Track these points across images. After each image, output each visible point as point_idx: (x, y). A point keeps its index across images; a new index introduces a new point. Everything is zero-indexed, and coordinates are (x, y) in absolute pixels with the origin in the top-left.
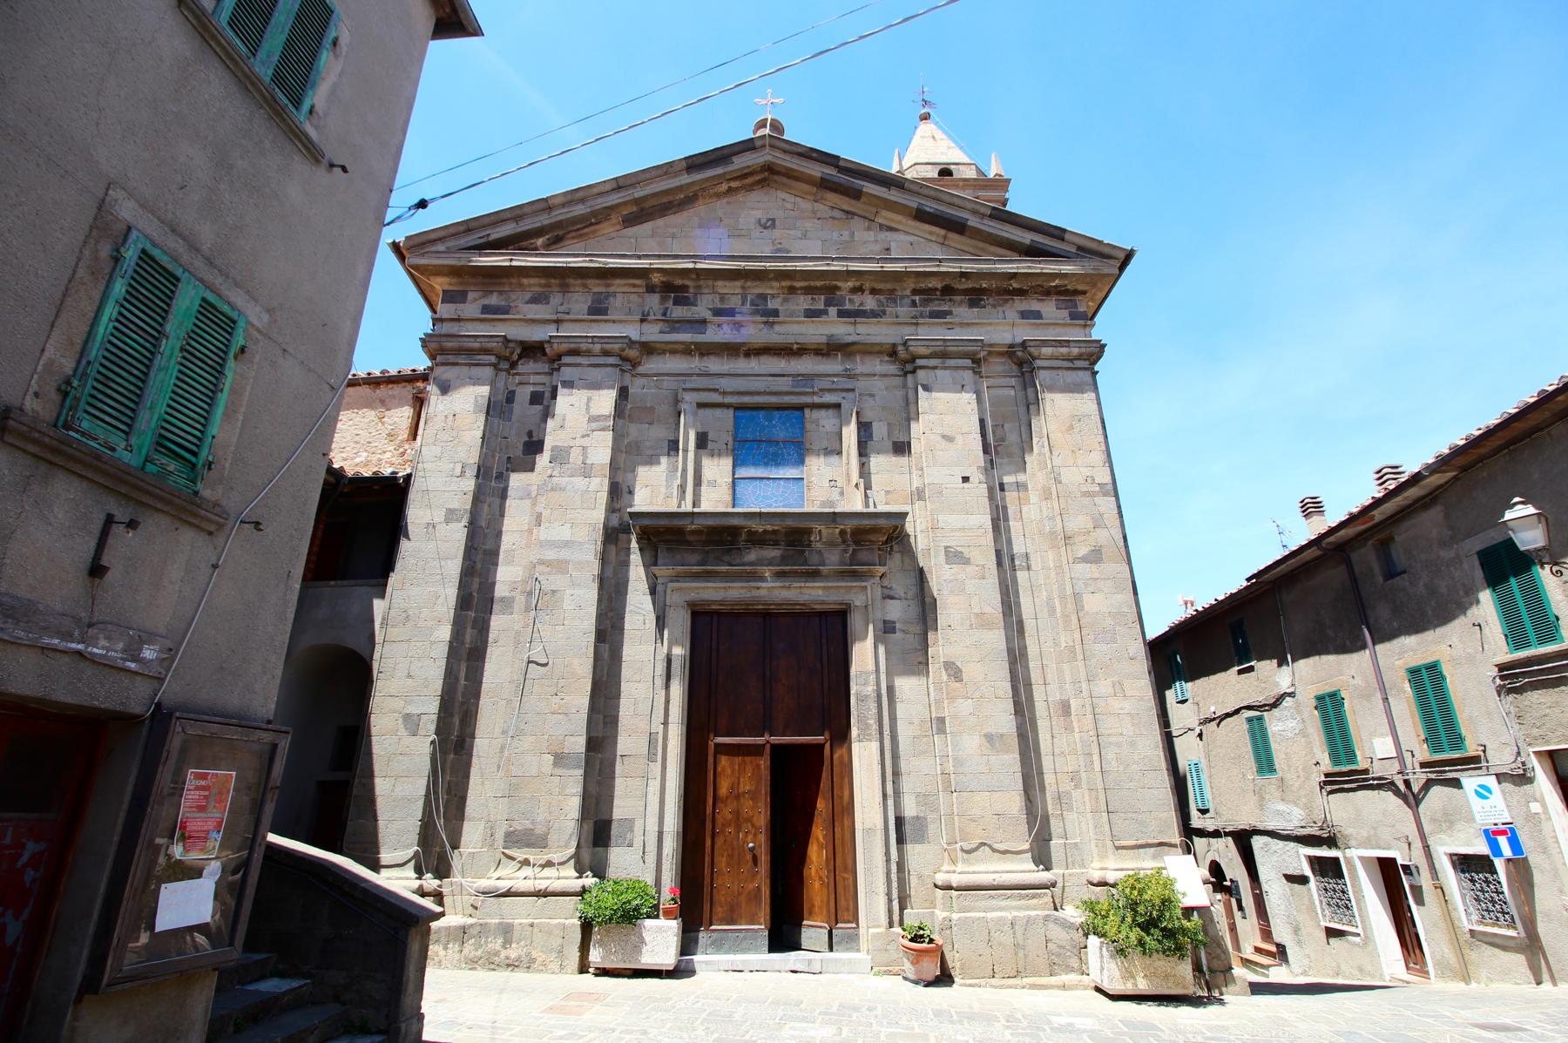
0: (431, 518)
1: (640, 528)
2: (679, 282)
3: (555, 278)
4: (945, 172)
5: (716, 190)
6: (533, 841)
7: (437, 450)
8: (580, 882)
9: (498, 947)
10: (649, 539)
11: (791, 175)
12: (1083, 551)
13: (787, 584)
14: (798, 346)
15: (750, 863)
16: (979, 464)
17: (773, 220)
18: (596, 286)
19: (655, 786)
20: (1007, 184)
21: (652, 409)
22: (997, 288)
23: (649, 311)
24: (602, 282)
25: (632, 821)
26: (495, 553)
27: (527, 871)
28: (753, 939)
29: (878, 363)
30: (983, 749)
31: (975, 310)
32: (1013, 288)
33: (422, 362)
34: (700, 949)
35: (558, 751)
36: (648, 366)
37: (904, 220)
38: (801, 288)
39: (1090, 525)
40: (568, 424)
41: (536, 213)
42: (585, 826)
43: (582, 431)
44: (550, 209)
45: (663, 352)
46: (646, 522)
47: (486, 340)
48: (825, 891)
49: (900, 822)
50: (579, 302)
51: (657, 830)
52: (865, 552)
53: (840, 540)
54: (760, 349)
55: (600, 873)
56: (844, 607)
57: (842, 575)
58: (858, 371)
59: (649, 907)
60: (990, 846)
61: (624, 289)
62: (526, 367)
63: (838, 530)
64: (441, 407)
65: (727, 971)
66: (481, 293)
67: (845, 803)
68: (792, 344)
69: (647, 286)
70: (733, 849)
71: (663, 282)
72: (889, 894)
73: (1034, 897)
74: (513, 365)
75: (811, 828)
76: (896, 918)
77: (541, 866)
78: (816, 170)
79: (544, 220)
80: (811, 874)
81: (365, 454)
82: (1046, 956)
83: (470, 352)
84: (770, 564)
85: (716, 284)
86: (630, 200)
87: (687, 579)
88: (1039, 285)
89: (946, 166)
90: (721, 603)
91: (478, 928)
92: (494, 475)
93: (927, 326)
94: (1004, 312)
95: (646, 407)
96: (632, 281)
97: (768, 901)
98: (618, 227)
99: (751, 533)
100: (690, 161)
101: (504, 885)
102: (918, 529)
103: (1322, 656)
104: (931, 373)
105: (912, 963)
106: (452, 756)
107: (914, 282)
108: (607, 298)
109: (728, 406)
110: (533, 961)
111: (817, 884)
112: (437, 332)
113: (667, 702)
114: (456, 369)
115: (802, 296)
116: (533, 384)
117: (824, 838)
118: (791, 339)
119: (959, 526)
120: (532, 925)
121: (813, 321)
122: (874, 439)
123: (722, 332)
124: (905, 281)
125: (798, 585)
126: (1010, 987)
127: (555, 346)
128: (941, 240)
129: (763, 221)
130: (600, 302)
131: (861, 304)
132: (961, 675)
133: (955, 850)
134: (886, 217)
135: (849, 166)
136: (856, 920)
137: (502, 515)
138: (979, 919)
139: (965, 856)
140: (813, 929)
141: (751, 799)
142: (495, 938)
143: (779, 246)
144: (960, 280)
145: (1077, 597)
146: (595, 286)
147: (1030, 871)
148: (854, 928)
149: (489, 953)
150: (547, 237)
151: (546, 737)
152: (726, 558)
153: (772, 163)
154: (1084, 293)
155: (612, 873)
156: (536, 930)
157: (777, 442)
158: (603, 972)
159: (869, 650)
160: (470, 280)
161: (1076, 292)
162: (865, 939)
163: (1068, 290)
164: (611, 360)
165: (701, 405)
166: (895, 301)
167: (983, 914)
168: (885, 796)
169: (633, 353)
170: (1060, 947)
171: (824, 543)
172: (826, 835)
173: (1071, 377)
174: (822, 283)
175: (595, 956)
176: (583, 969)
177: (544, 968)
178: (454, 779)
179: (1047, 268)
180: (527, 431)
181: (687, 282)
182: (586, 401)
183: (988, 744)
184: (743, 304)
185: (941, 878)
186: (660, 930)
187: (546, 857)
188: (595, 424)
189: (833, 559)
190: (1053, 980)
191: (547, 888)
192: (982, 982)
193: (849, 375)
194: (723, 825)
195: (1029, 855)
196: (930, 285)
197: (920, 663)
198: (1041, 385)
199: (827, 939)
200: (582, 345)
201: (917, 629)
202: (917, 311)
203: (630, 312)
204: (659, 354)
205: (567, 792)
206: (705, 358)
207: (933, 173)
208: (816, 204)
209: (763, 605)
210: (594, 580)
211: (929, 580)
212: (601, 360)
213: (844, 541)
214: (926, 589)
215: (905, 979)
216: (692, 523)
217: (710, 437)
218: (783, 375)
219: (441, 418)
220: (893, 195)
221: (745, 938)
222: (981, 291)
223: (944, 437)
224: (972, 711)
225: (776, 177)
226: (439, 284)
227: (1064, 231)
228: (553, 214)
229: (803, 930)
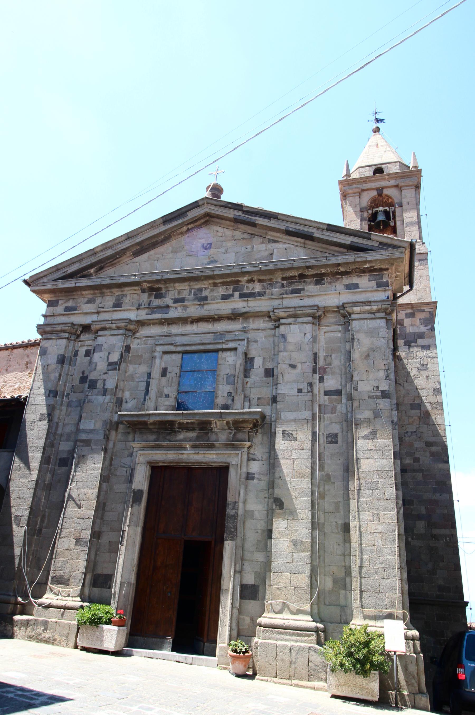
2: (156, 286)
3: (97, 290)
4: (378, 170)
6: (63, 582)
9: (41, 632)
18: (117, 292)
20: (419, 172)
22: (331, 272)
23: (142, 303)
29: (262, 322)
32: (341, 271)
33: (39, 337)
36: (141, 332)
37: (281, 236)
38: (220, 283)
39: (372, 417)
43: (105, 370)
44: (82, 260)
45: (150, 324)
50: (109, 301)
52: (241, 434)
53: (227, 427)
54: (198, 319)
58: (250, 328)
61: (131, 292)
62: (85, 337)
63: (225, 422)
66: (65, 300)
69: (141, 290)
71: (148, 287)
74: (78, 336)
79: (93, 260)
81: (19, 383)
83: (57, 332)
84: (190, 441)
85: (175, 285)
87: (148, 449)
89: (379, 166)
90: (164, 462)
92: (65, 395)
93: (288, 299)
94: (336, 286)
98: (131, 258)
99: (180, 424)
100: (164, 218)
103: (14, 533)
104: (288, 327)
106: (35, 537)
107: (281, 274)
108: (122, 298)
109: (179, 352)
110: (55, 640)
112: (47, 323)
114: (50, 341)
115: (221, 287)
116: (87, 346)
118: (212, 313)
120: (56, 622)
122: (255, 367)
125: (203, 452)
128: (303, 245)
129: (205, 245)
131: (253, 289)
134: (271, 235)
135: (248, 209)
138: (272, 644)
142: (40, 627)
143: (212, 259)
146: (117, 292)
147: (307, 621)
150: (96, 268)
151: (73, 530)
152: (168, 437)
153: (209, 212)
154: (387, 269)
158: (85, 649)
160: (59, 295)
161: (381, 270)
163: (376, 269)
164: (121, 332)
165: (165, 353)
166: (272, 285)
167: (275, 642)
169: (132, 327)
170: (316, 665)
171: (218, 429)
174: (230, 279)
177: (60, 644)
178: (35, 549)
180: (82, 371)
181: (160, 286)
183: (293, 546)
184: (189, 295)
189: (223, 437)
192: (269, 679)
193: (245, 331)
196: (291, 275)
197: (265, 498)
200: (107, 325)
202: (284, 290)
203: (132, 305)
204: (148, 325)
206: (170, 326)
207: (369, 173)
208: (234, 231)
209: (185, 463)
213: (229, 428)
216: (149, 419)
217: (169, 370)
218: (209, 333)
220: (272, 223)
222: (322, 275)
224: (287, 527)
225: (213, 219)
226: (47, 297)
228: (97, 256)
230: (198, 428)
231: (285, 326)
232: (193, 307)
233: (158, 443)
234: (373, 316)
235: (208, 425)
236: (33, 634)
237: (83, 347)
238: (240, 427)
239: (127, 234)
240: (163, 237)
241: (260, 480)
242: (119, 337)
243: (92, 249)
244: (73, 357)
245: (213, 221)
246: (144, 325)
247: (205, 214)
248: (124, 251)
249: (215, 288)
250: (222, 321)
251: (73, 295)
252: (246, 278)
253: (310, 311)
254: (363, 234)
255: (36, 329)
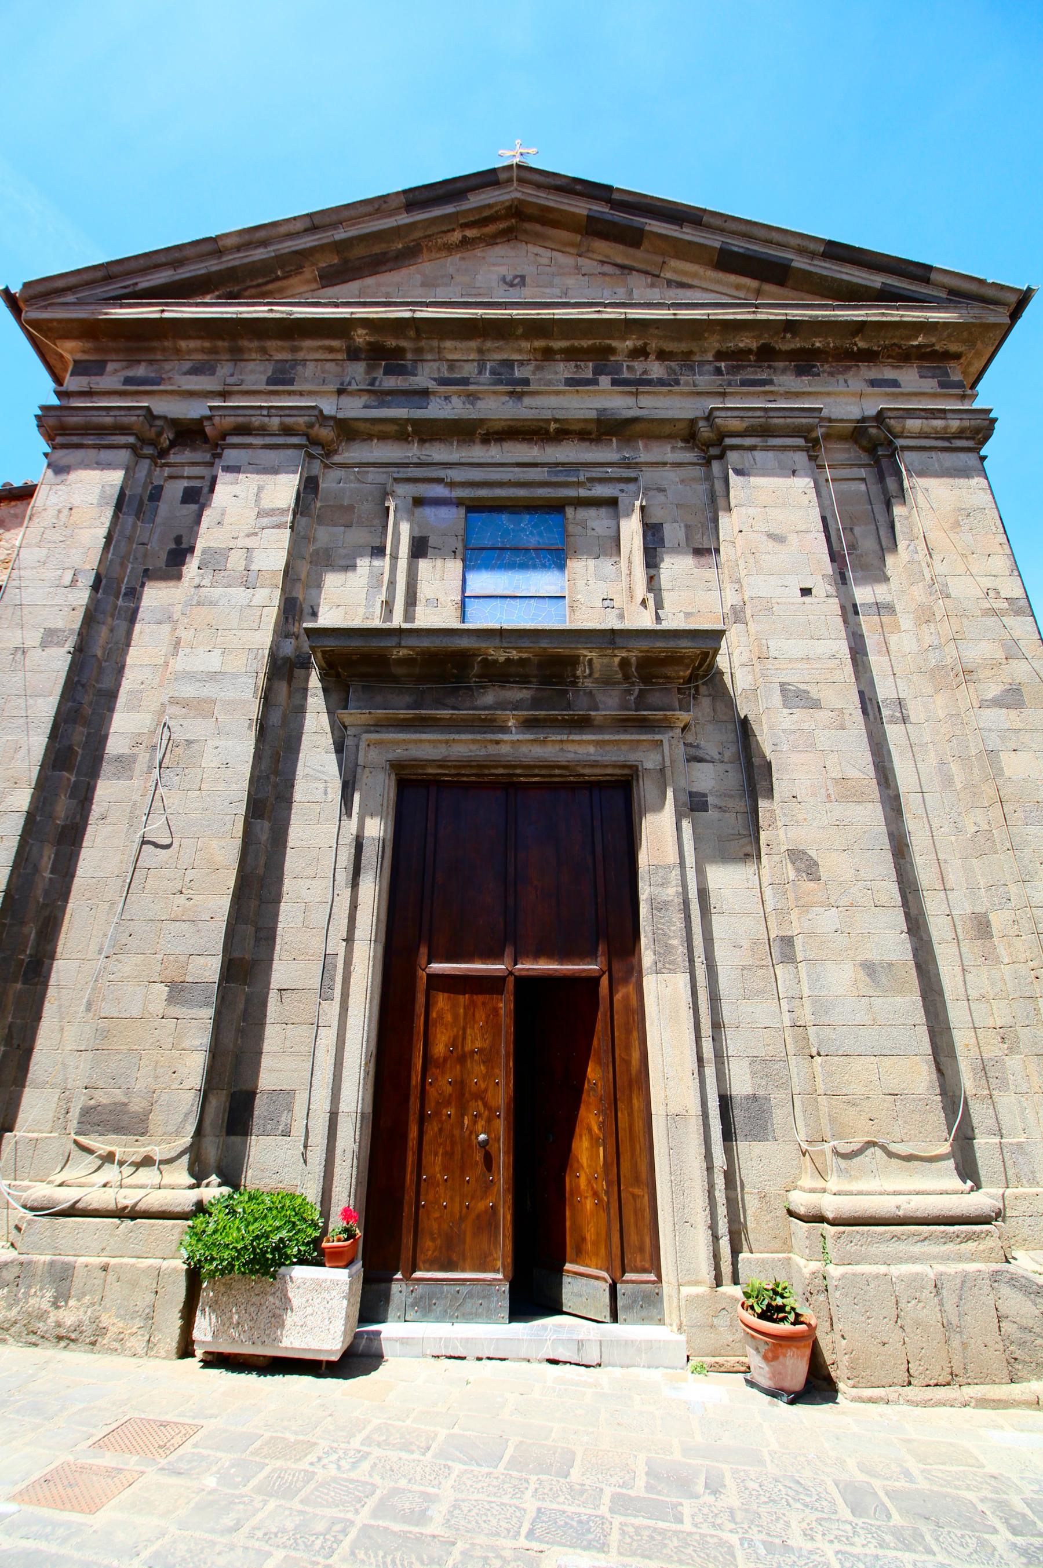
0: (21, 641)
1: (324, 653)
2: (391, 343)
3: (223, 340)
5: (445, 239)
6: (124, 1124)
7: (41, 553)
8: (194, 1195)
9: (45, 1305)
10: (338, 675)
11: (548, 218)
12: (993, 691)
13: (541, 737)
14: (557, 426)
15: (481, 1168)
16: (824, 572)
17: (523, 278)
19: (328, 1038)
21: (351, 508)
22: (836, 348)
24: (286, 344)
25: (290, 1094)
26: (111, 696)
27: (111, 1172)
28: (484, 1297)
29: (669, 450)
30: (860, 985)
31: (804, 378)
32: (859, 349)
34: (392, 1311)
35: (176, 979)
36: (346, 455)
39: (1000, 655)
40: (227, 520)
41: (202, 257)
42: (214, 1102)
45: (369, 437)
46: (331, 643)
47: (123, 413)
48: (603, 1215)
49: (725, 1102)
51: (328, 1109)
52: (657, 694)
53: (620, 676)
55: (231, 1178)
56: (626, 771)
57: (624, 724)
58: (642, 460)
59: (303, 1244)
60: (883, 1148)
61: (317, 356)
63: (617, 660)
64: (53, 499)
65: (438, 1357)
66: (124, 364)
67: (634, 1071)
68: (547, 421)
70: (453, 1143)
71: (369, 343)
72: (713, 1227)
73: (968, 1238)
74: (163, 453)
75: (578, 1111)
76: (726, 1268)
77: (132, 1164)
78: (581, 208)
79: (213, 266)
80: (578, 1186)
82: (1000, 1346)
83: (101, 430)
85: (442, 346)
86: (328, 244)
88: (894, 344)
90: (442, 764)
91: (15, 1270)
92: (123, 590)
95: (342, 506)
96: (327, 343)
97: (509, 1232)
98: (314, 286)
99: (486, 663)
101: (66, 1196)
102: (736, 664)
104: (748, 455)
105: (765, 1358)
106: (19, 986)
107: (718, 341)
108: (293, 367)
110: (103, 1331)
111: (589, 1204)
113: (354, 906)
115: (562, 364)
117: (600, 1129)
119: (800, 655)
120: (105, 1268)
121: (577, 391)
123: (450, 406)
124: (706, 339)
125: (559, 738)
126: (942, 1403)
127: (217, 420)
129: (508, 279)
130: (283, 372)
131: (645, 372)
132: (818, 870)
133: (822, 1152)
135: (626, 198)
136: (656, 1267)
137: (128, 645)
138: (877, 1277)
139: (843, 1163)
140: (584, 1280)
141: (484, 1062)
142: (41, 1290)
144: (784, 337)
145: (992, 754)
146: (277, 350)
147: (955, 1193)
148: (653, 1282)
149: (29, 1314)
151: (159, 957)
152: (450, 701)
153: (522, 202)
154: (957, 356)
155: (252, 1178)
156: (111, 1277)
157: (527, 549)
158: (217, 1361)
159: (670, 844)
160: (110, 344)
162: (675, 1304)
163: (936, 351)
165: (419, 502)
167: (883, 1269)
168: (700, 1060)
169: (326, 433)
170: (1023, 1329)
171: (597, 681)
172: (603, 1123)
173: (949, 459)
174: (590, 342)
175: (204, 1329)
176: (186, 1350)
179: (908, 316)
181: (404, 343)
182: (255, 491)
183: (868, 979)
184: (480, 373)
185: (801, 1201)
186: (318, 1286)
187: (142, 1151)
188: (266, 519)
190: (1016, 1390)
191: (136, 1204)
194: (438, 1103)
195: (951, 1163)
196: (741, 345)
198: (907, 470)
199: (607, 1300)
201: (741, 805)
202: (722, 380)
204: (364, 440)
205: (186, 1044)
206: (427, 445)
208: (579, 259)
209: (504, 767)
210: (250, 727)
211: (757, 733)
212: (280, 440)
213: (627, 677)
214: (754, 745)
215: (751, 1383)
219: (52, 512)
220: (687, 234)
221: (470, 1295)
223: (770, 536)
225: (528, 226)
227: (929, 268)
228: (224, 259)
229: (566, 1280)
230: (536, 676)
231: (741, 452)
232: (493, 398)
233: (423, 712)
234: (946, 444)
235: (569, 668)
236: (13, 1314)
237: (178, 481)
238: (657, 677)
239: (310, 216)
240: (400, 246)
241: (725, 811)
242: (290, 452)
243: (211, 238)
244: (146, 502)
245: (526, 232)
246: (354, 440)
247: (510, 207)
248: (303, 256)
249: (546, 363)
250: (564, 443)
251: (152, 350)
252: (629, 344)
253: (804, 421)
254: (912, 268)
255: (36, 422)
